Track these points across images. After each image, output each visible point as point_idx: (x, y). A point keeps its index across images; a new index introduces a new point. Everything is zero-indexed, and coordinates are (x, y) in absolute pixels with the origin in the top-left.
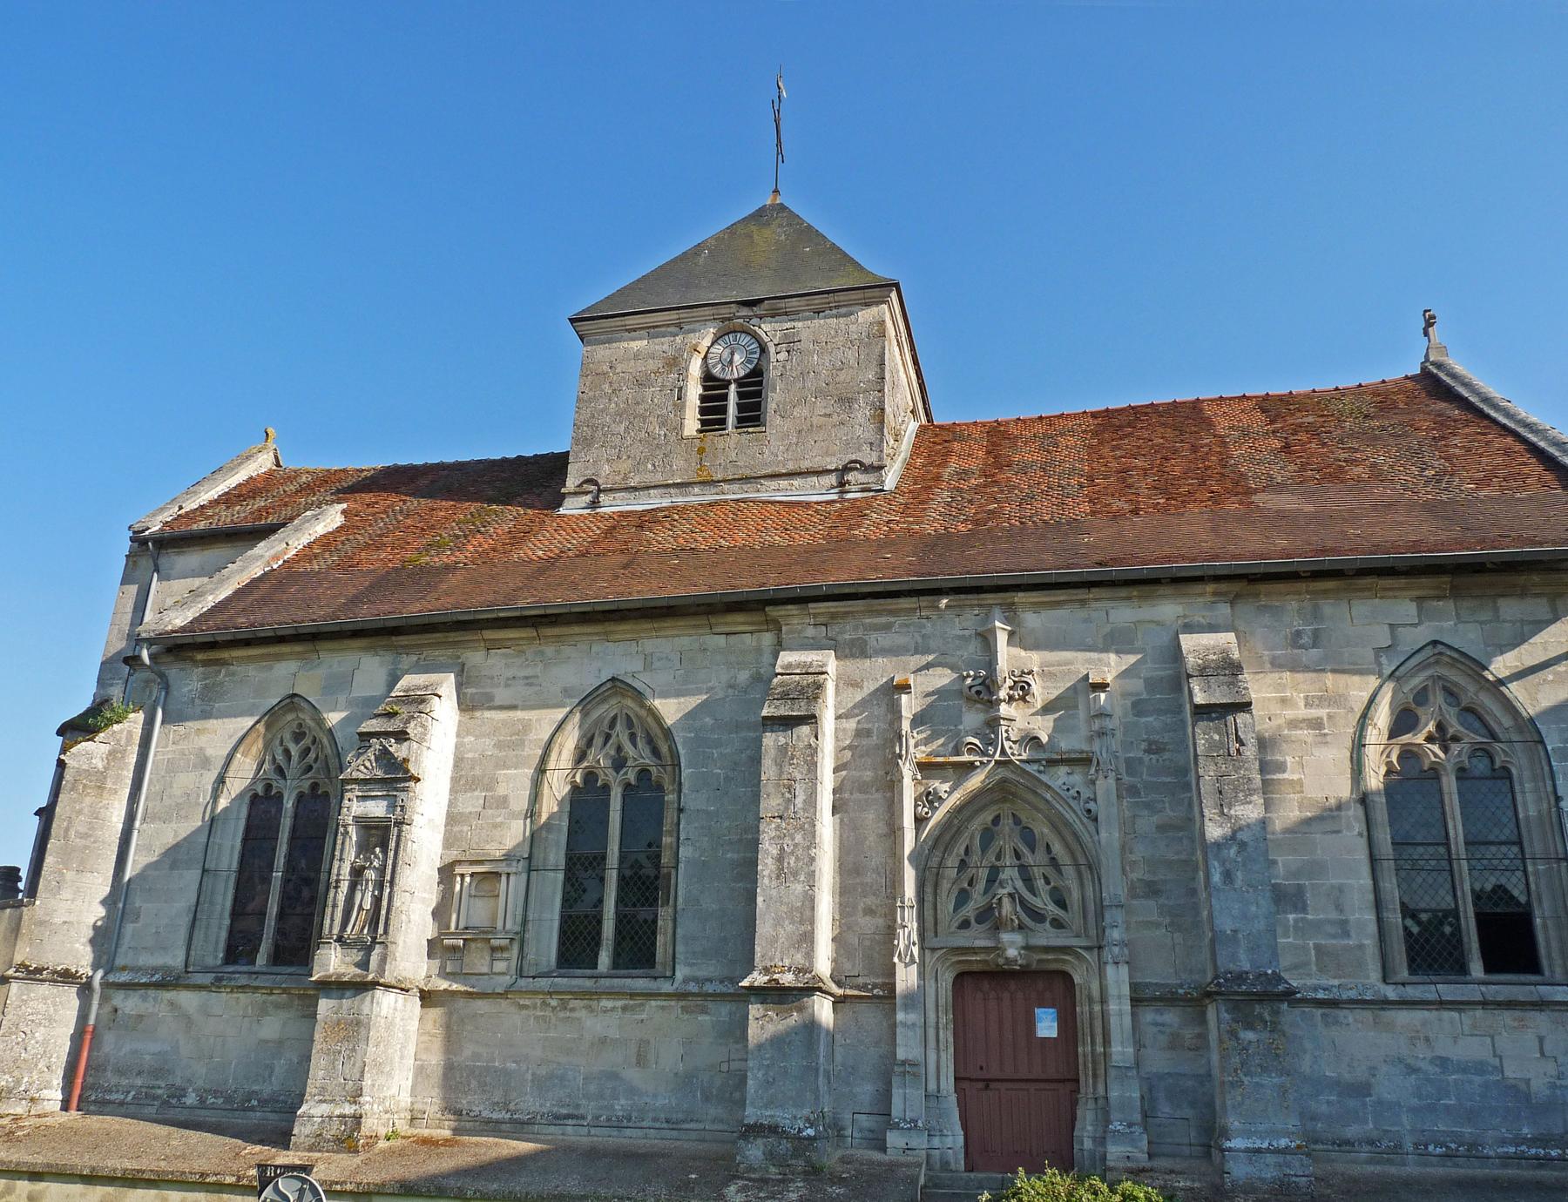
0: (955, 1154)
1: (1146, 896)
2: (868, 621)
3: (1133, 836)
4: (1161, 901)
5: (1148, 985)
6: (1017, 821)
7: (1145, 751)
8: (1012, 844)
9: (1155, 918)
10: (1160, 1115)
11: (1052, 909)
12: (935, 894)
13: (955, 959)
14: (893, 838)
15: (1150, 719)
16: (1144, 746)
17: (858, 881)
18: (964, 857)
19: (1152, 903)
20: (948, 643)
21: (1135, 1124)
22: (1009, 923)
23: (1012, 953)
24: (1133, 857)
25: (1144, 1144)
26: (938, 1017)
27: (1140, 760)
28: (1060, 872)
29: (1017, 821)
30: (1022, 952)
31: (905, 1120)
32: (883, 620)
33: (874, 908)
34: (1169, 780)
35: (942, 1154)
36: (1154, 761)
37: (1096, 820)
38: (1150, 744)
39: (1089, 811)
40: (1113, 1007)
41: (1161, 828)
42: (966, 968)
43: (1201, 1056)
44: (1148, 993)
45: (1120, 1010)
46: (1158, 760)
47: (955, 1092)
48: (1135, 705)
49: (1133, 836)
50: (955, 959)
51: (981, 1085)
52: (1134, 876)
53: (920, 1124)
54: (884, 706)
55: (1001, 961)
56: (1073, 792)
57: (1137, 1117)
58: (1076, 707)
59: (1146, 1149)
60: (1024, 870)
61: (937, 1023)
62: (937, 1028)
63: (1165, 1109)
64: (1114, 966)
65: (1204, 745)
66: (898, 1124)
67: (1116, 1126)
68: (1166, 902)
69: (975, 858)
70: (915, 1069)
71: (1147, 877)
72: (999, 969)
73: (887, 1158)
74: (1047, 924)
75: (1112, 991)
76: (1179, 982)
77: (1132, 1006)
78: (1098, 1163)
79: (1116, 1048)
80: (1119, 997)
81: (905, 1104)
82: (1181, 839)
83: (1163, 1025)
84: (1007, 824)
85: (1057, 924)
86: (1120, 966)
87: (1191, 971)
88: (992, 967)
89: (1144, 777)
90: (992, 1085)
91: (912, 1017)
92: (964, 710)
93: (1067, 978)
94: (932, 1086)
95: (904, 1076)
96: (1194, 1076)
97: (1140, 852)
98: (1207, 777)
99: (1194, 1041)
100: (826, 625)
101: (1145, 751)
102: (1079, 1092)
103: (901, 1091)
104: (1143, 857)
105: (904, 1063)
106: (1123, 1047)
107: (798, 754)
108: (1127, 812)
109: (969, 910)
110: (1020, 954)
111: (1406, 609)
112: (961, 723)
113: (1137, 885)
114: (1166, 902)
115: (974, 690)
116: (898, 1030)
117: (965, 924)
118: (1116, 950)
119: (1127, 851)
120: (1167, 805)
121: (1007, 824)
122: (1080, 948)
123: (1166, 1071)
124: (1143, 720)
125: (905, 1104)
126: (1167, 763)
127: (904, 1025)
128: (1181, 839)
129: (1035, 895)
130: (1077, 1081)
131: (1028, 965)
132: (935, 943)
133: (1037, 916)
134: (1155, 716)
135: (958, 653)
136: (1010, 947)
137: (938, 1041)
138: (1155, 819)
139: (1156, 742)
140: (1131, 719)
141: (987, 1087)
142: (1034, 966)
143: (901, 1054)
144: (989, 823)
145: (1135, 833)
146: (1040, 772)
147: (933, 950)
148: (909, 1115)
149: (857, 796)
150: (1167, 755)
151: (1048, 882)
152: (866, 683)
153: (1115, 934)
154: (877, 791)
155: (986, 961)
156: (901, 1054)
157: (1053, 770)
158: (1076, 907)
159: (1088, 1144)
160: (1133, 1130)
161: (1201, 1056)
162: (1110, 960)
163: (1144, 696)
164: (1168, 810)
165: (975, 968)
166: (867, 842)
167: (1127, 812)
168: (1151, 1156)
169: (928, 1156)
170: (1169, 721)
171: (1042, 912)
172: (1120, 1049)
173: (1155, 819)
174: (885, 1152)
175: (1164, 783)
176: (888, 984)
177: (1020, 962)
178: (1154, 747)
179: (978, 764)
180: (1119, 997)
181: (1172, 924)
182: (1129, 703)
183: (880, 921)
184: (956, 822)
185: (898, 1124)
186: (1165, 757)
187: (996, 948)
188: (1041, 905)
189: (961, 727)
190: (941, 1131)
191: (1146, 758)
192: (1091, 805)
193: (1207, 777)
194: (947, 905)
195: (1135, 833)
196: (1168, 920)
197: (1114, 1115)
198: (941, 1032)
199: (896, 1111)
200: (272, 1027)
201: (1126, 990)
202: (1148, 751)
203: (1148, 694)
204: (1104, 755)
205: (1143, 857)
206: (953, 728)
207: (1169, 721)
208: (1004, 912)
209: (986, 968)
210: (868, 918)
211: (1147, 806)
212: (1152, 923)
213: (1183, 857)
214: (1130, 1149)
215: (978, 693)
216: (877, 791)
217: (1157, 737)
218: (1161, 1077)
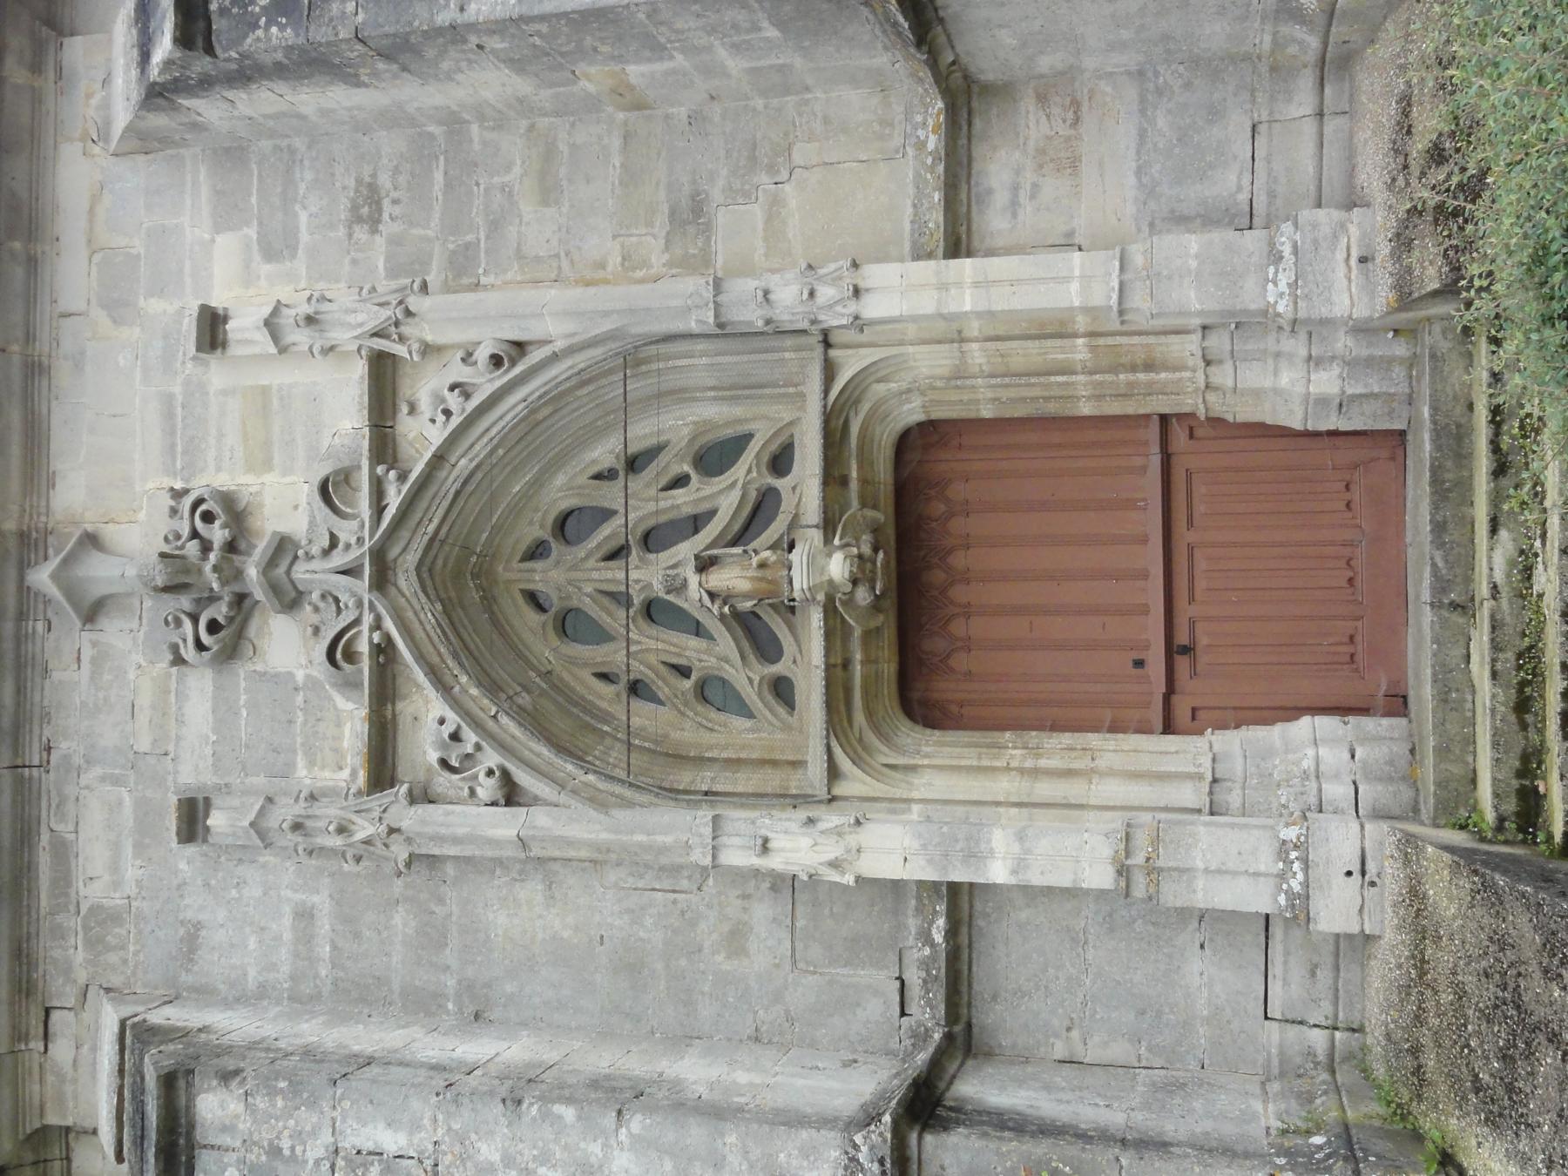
0: (1366, 739)
1: (707, 230)
2: (44, 902)
3: (565, 264)
4: (717, 195)
5: (918, 222)
6: (537, 552)
7: (374, 231)
8: (591, 563)
9: (757, 211)
10: (1243, 197)
11: (745, 472)
12: (701, 761)
13: (859, 717)
14: (556, 866)
15: (303, 217)
16: (361, 233)
17: (659, 966)
18: (622, 686)
19: (722, 219)
20: (106, 699)
21: (1272, 244)
22: (768, 574)
23: (838, 567)
24: (614, 261)
25: (1326, 217)
26: (1008, 769)
27: (395, 241)
28: (652, 453)
29: (537, 552)
30: (837, 542)
31: (1282, 877)
32: (44, 860)
33: (726, 928)
34: (439, 177)
35: (1368, 777)
36: (397, 210)
37: (520, 347)
38: (359, 220)
39: (496, 361)
40: (966, 302)
41: (548, 193)
42: (889, 689)
43: (1091, 91)
44: (935, 219)
45: (976, 285)
46: (395, 202)
47: (1201, 733)
48: (270, 254)
49: (565, 264)
50: (859, 717)
51: (1182, 663)
52: (658, 260)
53: (1291, 833)
54: (241, 870)
55: (863, 596)
56: (453, 400)
57: (1253, 241)
58: (265, 391)
59: (1337, 215)
60: (653, 540)
61: (1022, 771)
62: (1036, 773)
63: (1229, 183)
64: (866, 299)
65: (282, 28)
66: (1290, 895)
67: (1277, 296)
68: (721, 183)
69: (612, 655)
70: (1142, 840)
71: (661, 223)
72: (890, 604)
73: (1389, 936)
74: (782, 484)
75: (926, 304)
76: (910, 151)
77: (969, 254)
78: (1378, 352)
79: (1072, 295)
80: (943, 287)
81: (1235, 874)
82: (574, 147)
83: (1016, 188)
84: (547, 577)
85: (780, 462)
86: (862, 285)
87: (886, 123)
88: (886, 622)
89: (430, 233)
90: (1182, 638)
91: (1000, 841)
92: (259, 667)
93: (904, 441)
94: (1190, 795)
95: (1160, 870)
96: (1143, 111)
97: (601, 244)
98: (360, 18)
99: (1056, 111)
100: (47, 1011)
101: (374, 231)
102: (1192, 415)
103: (1200, 883)
104: (614, 237)
105: (1123, 871)
106: (1067, 279)
107: (266, 1136)
108: (509, 276)
109: (746, 677)
110: (844, 546)
111: (1325, 1046)
112: (291, 675)
113: (679, 252)
114: (721, 183)
115: (206, 639)
116: (1036, 879)
117: (782, 690)
118: (826, 293)
119: (600, 274)
120: (496, 180)
121: (547, 577)
122: (826, 392)
123: (1132, 180)
124: (304, 237)
125: (1235, 874)
126: (402, 179)
127: (1019, 866)
128: (574, 147)
129: (712, 513)
130: (1164, 419)
131: (876, 530)
132: (816, 769)
133: (761, 508)
134: (297, 207)
135: (132, 676)
136: (823, 570)
137: (1069, 773)
138: (527, 208)
139: (355, 208)
140: (300, 265)
141: (1186, 650)
142: (882, 515)
143: (1100, 877)
144: (543, 617)
145: (557, 256)
146: (402, 477)
147: (833, 773)
148: (1267, 861)
149: (450, 956)
150: (384, 180)
151: (680, 481)
152: (189, 915)
153: (788, 296)
154: (441, 901)
155: (868, 635)
156: (1100, 877)
157: (405, 450)
158: (738, 411)
159: (1327, 382)
160: (1287, 250)
161: (1091, 91)
162: (852, 307)
163: (252, 232)
164: (506, 179)
165: (889, 668)
166: (566, 934)
167: (509, 276)
168: (1353, 201)
169: (1379, 815)
170: (309, 175)
171: (753, 495)
172: (1075, 286)
173: (527, 208)
174: (1368, 938)
175: (449, 186)
176: (919, 898)
177: (866, 550)
178: (365, 210)
179: (376, 637)
180: (943, 287)
181: (772, 169)
182: (266, 268)
183: (763, 912)
184: (525, 700)
185: (1290, 895)
186: (388, 185)
187: (830, 610)
188: (735, 495)
189: (300, 675)
190: (1305, 775)
191: (387, 227)
192: (482, 355)
193: (360, 18)
194: (734, 735)
195: (557, 256)
196: (764, 178)
197: (1249, 299)
198: (1043, 763)
199: (1259, 899)
200: (1174, 420)
201: (927, 269)
202: (374, 223)
203: (247, 224)
204: (361, 317)
205: (614, 237)
206: (300, 699)
207: (309, 175)
208: (744, 585)
209: (889, 636)
210: (753, 945)
211: (495, 226)
212: (769, 220)
213: (616, 143)
214: (1340, 255)
215: (214, 627)
216: (441, 901)
217: (344, 204)
218: (1149, 191)
